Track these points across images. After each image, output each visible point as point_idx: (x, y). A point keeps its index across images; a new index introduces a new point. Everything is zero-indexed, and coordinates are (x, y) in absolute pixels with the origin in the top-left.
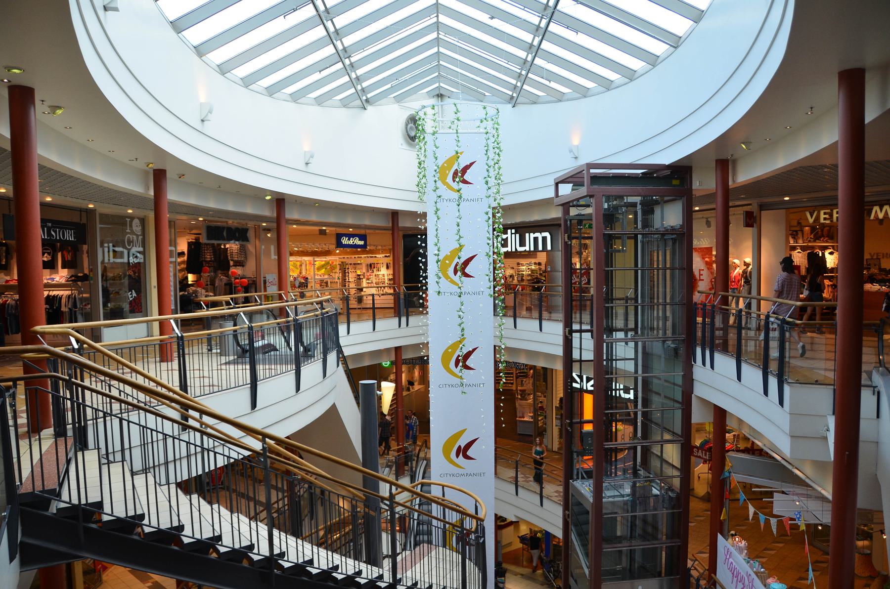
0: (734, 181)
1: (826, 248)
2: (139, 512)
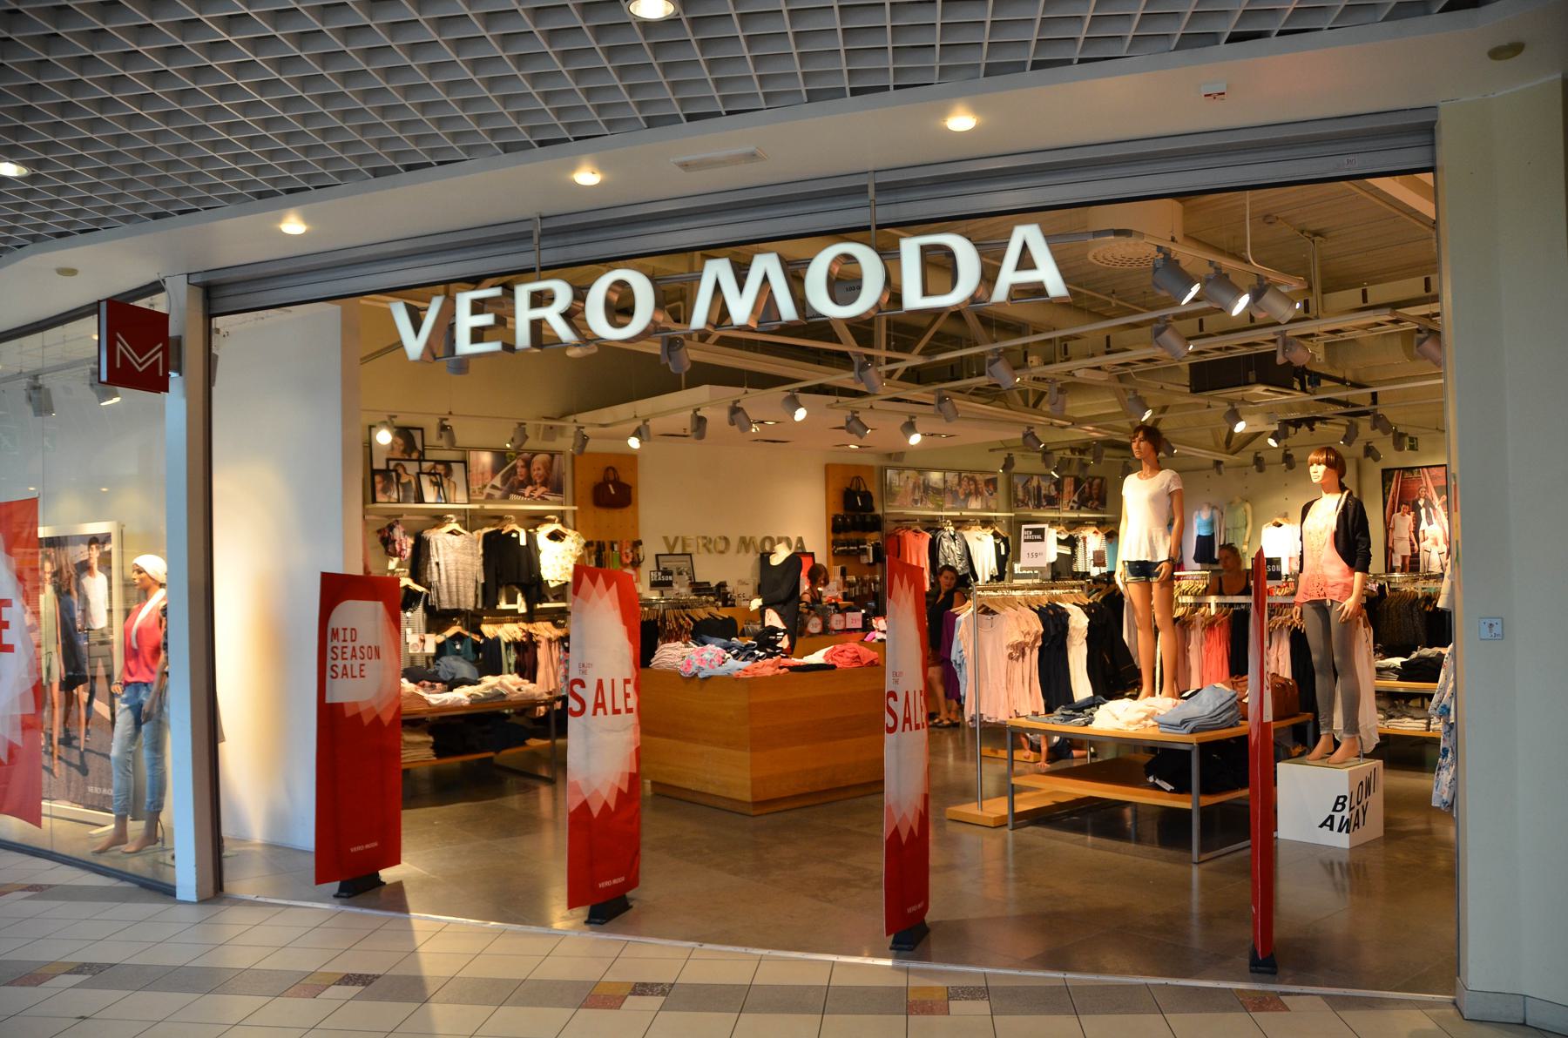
0: (1006, 841)
1: (538, 519)
2: (45, 821)
